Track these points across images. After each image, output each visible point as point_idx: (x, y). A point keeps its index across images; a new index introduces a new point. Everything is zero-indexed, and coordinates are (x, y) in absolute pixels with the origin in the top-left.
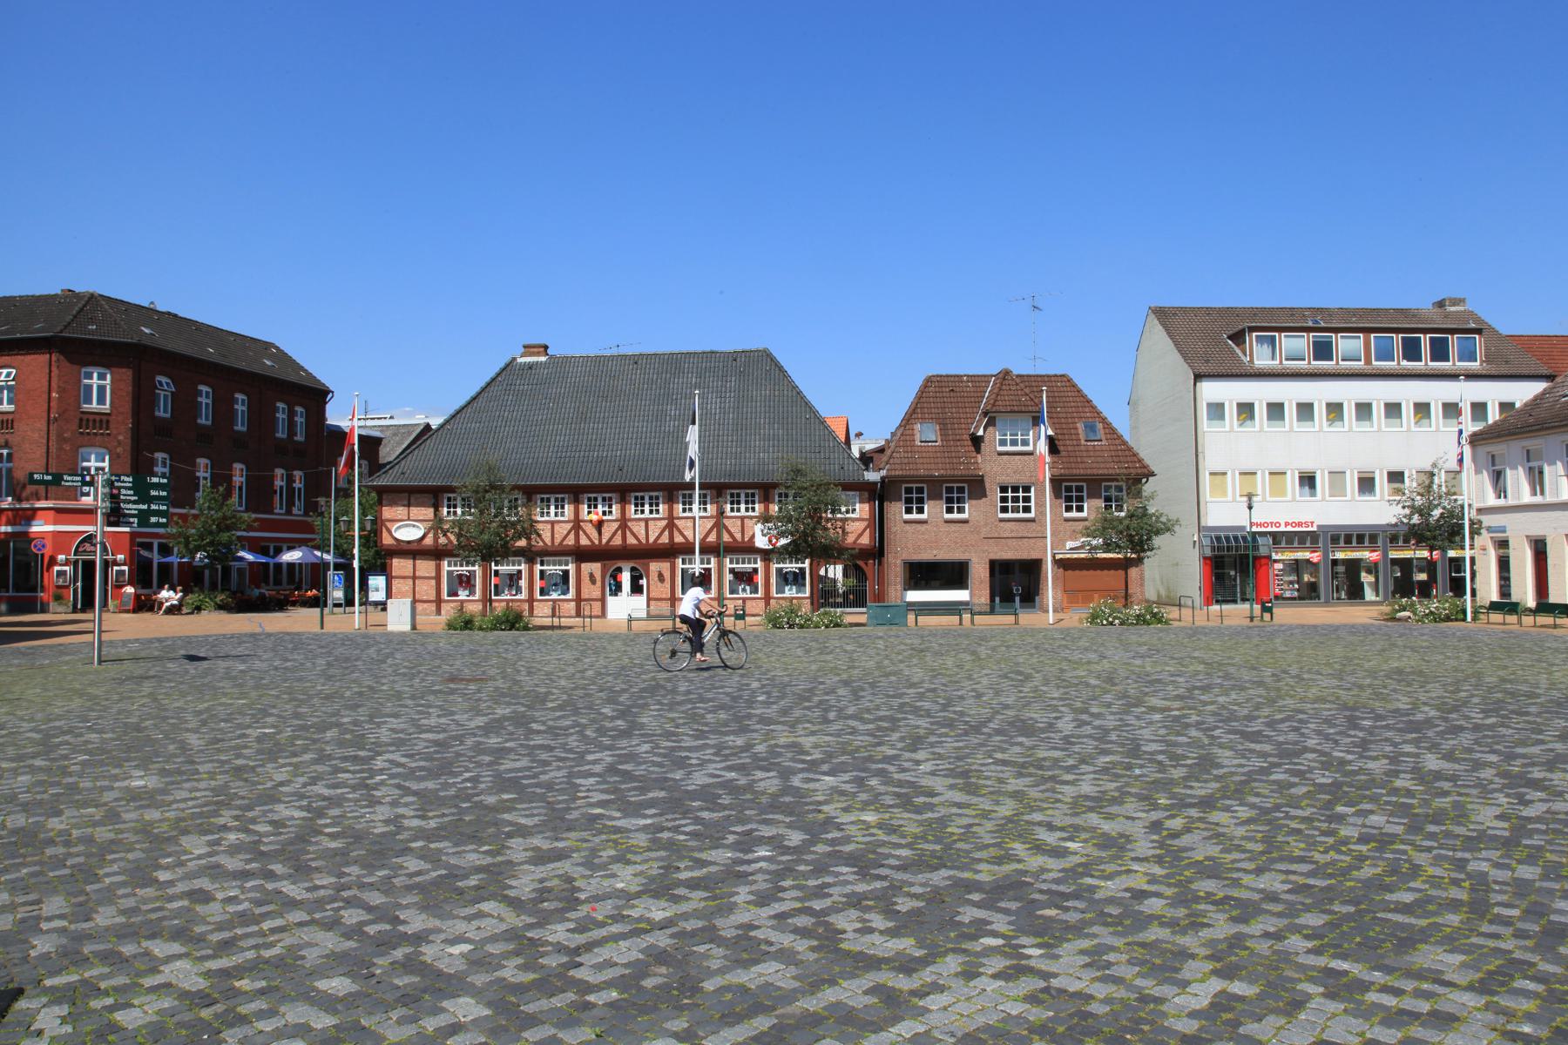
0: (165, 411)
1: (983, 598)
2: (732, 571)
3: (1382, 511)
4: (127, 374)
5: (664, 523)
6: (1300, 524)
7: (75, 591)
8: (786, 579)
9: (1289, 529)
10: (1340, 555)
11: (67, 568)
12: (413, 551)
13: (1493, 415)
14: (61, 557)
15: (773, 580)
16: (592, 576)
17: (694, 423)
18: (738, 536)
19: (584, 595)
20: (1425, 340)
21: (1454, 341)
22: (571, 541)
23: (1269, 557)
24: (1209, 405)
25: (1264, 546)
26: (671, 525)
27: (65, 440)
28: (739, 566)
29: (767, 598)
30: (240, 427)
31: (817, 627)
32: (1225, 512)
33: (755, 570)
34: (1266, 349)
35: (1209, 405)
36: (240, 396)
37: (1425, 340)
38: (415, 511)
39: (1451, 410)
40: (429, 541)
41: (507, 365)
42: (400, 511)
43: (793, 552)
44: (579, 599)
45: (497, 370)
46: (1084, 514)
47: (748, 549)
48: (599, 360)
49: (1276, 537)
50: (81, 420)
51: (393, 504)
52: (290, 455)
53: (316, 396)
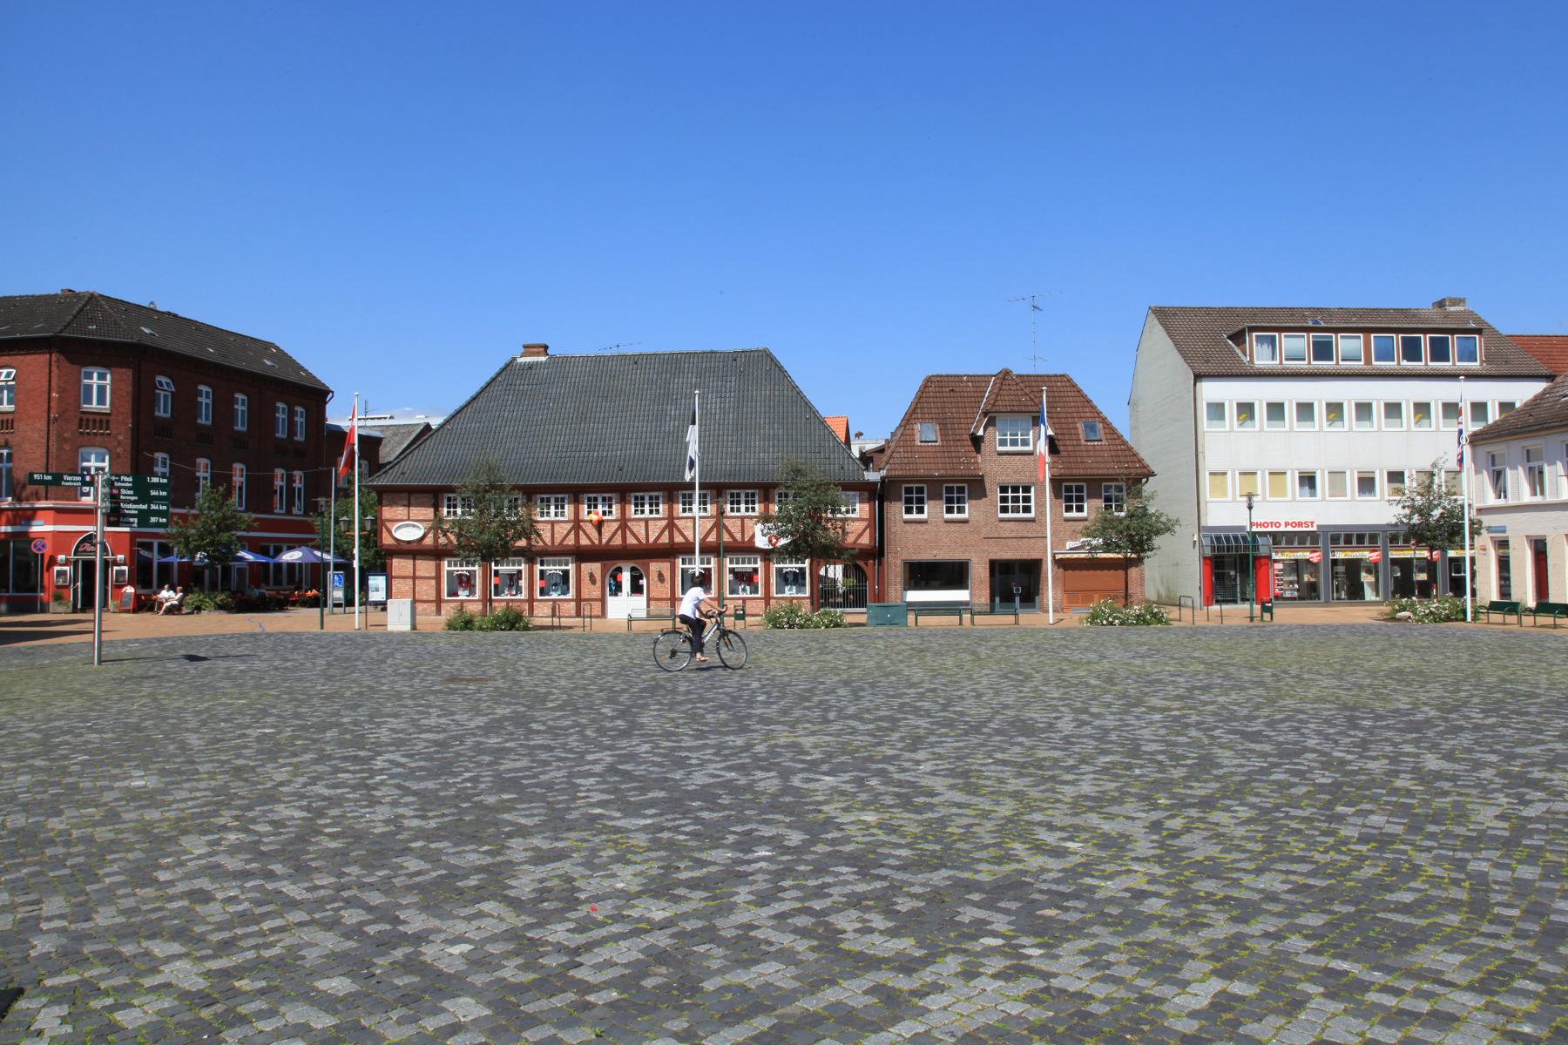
0: (165, 411)
1: (983, 598)
2: (732, 571)
3: (1382, 511)
4: (127, 374)
5: (664, 523)
6: (1300, 524)
7: (75, 591)
8: (786, 579)
9: (1289, 529)
10: (1340, 555)
11: (67, 568)
12: (413, 551)
13: (1493, 415)
14: (61, 557)
15: (773, 580)
16: (592, 576)
17: (694, 423)
18: (738, 536)
19: (584, 595)
20: (1425, 340)
21: (1454, 341)
22: (571, 541)
23: (1269, 557)
24: (1209, 405)
25: (1264, 546)
26: (671, 525)
27: (65, 440)
28: (739, 566)
29: (767, 598)
30: (240, 427)
31: (817, 627)
32: (1225, 512)
33: (755, 570)
34: (1266, 349)
35: (1209, 405)
36: (240, 396)
37: (1425, 340)
38: (415, 511)
39: (1451, 410)
40: (429, 541)
41: (507, 365)
42: (400, 511)
43: (793, 552)
44: (579, 599)
45: (497, 370)
46: (1084, 514)
47: (748, 549)
48: (599, 360)
49: (1276, 537)
50: (81, 420)
51: (393, 504)
52: (290, 455)
53: (316, 396)
